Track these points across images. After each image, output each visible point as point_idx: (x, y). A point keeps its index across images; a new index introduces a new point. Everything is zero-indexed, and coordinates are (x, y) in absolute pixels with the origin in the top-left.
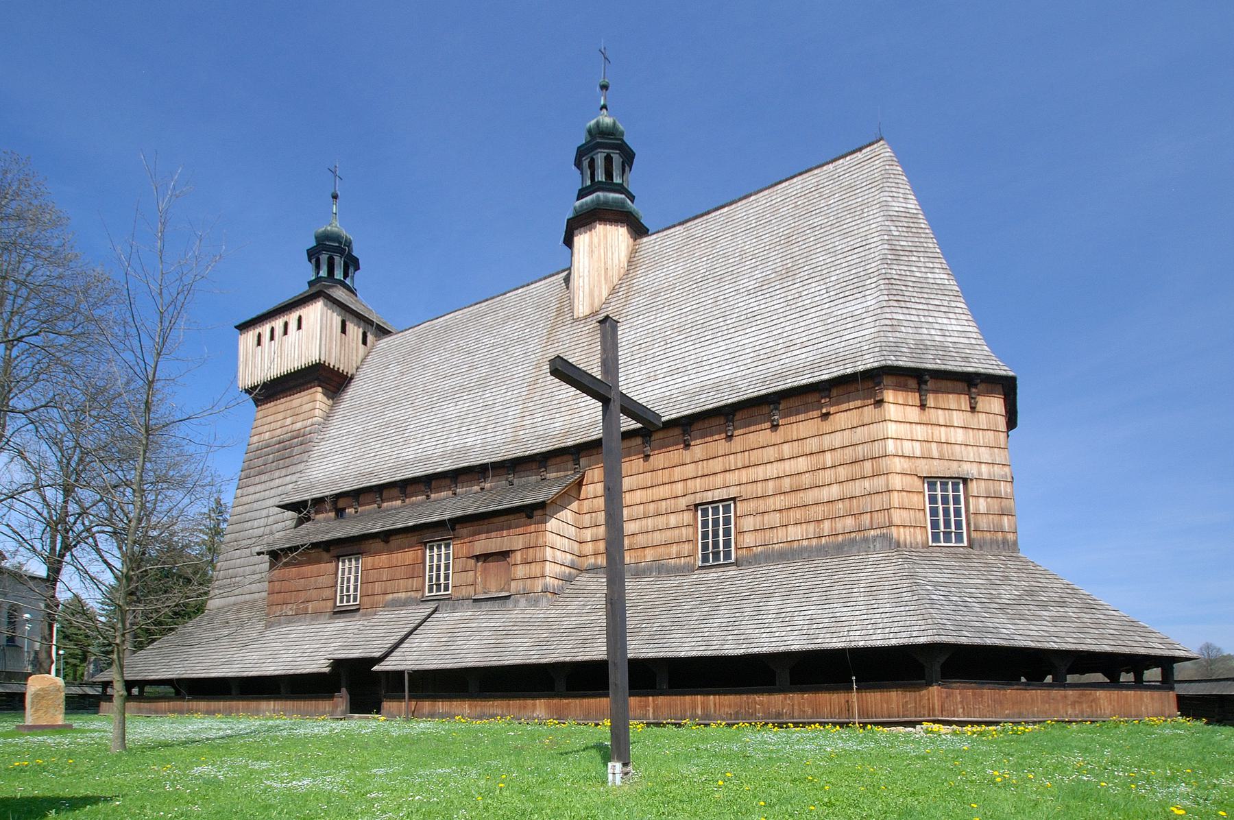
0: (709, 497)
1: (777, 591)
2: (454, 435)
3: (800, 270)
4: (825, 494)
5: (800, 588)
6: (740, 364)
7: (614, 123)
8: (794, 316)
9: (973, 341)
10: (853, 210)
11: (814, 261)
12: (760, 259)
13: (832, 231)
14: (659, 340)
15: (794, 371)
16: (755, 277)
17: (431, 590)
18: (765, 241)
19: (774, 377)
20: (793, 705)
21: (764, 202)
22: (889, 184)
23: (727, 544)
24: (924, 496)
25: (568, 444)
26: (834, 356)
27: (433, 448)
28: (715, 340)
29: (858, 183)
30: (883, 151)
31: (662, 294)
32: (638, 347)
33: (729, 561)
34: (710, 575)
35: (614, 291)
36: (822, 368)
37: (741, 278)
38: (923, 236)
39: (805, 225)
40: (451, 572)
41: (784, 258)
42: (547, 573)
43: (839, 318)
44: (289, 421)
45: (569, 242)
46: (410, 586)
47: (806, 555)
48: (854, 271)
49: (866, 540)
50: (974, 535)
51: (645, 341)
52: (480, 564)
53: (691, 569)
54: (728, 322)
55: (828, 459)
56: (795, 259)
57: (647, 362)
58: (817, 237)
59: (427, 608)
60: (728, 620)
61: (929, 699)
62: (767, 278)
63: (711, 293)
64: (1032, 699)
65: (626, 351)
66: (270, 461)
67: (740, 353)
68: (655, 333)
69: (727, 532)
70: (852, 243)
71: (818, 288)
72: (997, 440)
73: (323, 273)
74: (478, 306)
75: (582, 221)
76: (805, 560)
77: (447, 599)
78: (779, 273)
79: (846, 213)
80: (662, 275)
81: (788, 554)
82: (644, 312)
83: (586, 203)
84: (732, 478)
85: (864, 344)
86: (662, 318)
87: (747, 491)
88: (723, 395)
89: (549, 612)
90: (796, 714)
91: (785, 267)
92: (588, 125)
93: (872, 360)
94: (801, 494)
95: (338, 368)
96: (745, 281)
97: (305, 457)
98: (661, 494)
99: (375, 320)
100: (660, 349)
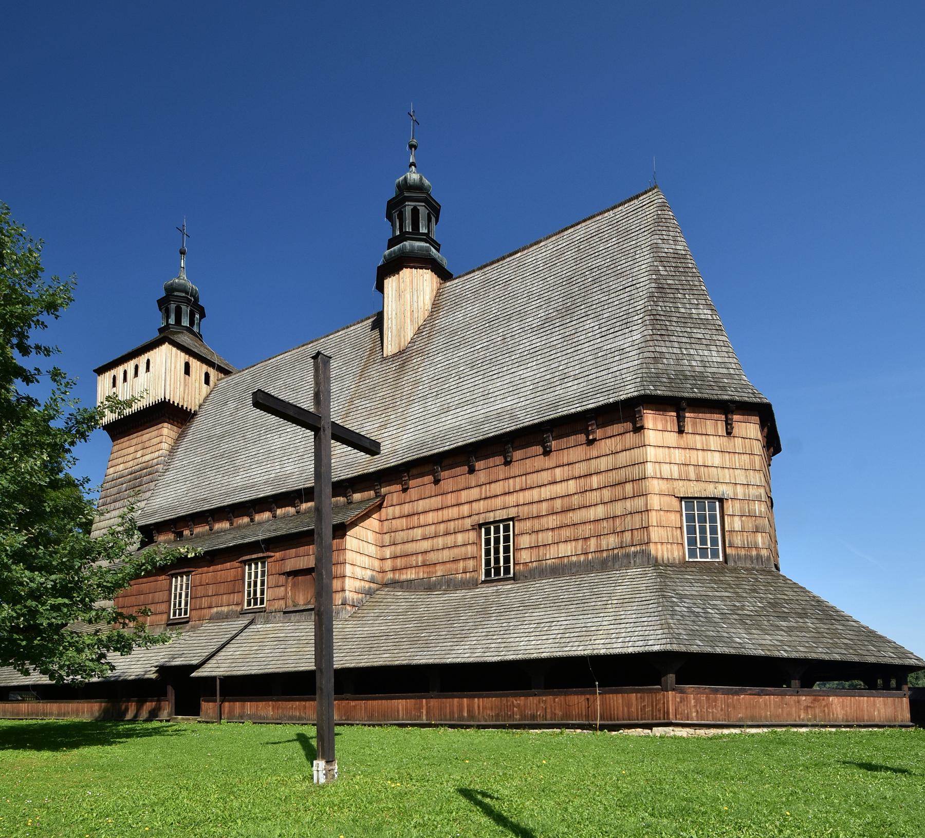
0: (491, 517)
1: (543, 603)
2: (277, 464)
3: (578, 309)
4: (592, 513)
5: (563, 600)
6: (521, 395)
7: (421, 179)
8: (569, 351)
9: (732, 371)
10: (627, 253)
11: (590, 300)
12: (544, 299)
13: (608, 272)
14: (453, 375)
15: (565, 402)
16: (539, 316)
17: (249, 604)
18: (550, 282)
19: (548, 407)
20: (546, 708)
21: (552, 247)
22: (659, 228)
23: (507, 560)
24: (681, 515)
25: (370, 471)
26: (601, 387)
27: (258, 476)
28: (501, 375)
29: (633, 227)
30: (656, 198)
31: (459, 333)
32: (435, 382)
33: (508, 576)
34: (490, 589)
35: (419, 332)
36: (590, 398)
37: (527, 317)
38: (690, 275)
39: (584, 267)
40: (266, 587)
41: (565, 298)
42: (347, 587)
43: (608, 352)
44: (139, 454)
45: (380, 288)
46: (231, 600)
47: (574, 570)
48: (624, 309)
49: (627, 555)
50: (728, 551)
51: (442, 376)
52: (291, 578)
53: (475, 584)
54: (513, 358)
55: (595, 481)
56: (574, 298)
57: (443, 395)
58: (594, 278)
59: (243, 621)
60: (495, 629)
61: (664, 703)
62: (549, 316)
63: (500, 331)
64: (765, 704)
65: (425, 386)
66: (124, 490)
67: (522, 385)
68: (450, 369)
69: (506, 549)
70: (624, 283)
71: (592, 325)
72: (752, 462)
73: (172, 321)
74: (305, 347)
75: (391, 267)
76: (574, 574)
77: (263, 611)
78: (560, 312)
79: (620, 255)
80: (460, 316)
81: (559, 570)
82: (443, 350)
83: (394, 250)
84: (511, 500)
85: (628, 375)
86: (458, 355)
87: (524, 511)
88: (503, 424)
89: (347, 623)
90: (548, 717)
91: (565, 306)
92: (397, 181)
93: (632, 390)
94: (571, 514)
95: (182, 406)
96: (530, 319)
97: (152, 485)
98: (450, 515)
99: (216, 362)
100: (454, 383)
